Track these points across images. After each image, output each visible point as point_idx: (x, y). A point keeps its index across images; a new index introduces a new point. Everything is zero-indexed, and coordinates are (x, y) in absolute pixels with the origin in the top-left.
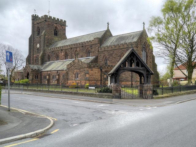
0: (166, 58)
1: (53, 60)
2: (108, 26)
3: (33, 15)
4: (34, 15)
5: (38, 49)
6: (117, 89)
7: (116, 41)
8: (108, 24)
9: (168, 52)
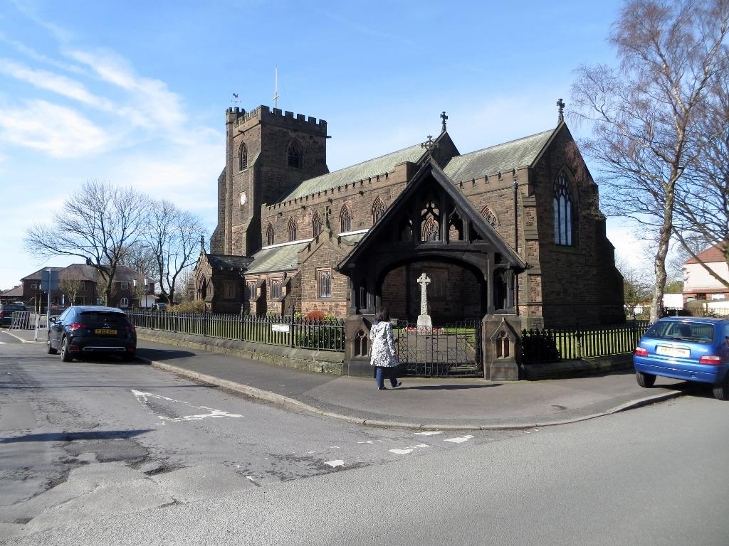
0: (646, 217)
2: (444, 123)
4: (233, 110)
7: (468, 171)
8: (444, 117)
9: (645, 196)
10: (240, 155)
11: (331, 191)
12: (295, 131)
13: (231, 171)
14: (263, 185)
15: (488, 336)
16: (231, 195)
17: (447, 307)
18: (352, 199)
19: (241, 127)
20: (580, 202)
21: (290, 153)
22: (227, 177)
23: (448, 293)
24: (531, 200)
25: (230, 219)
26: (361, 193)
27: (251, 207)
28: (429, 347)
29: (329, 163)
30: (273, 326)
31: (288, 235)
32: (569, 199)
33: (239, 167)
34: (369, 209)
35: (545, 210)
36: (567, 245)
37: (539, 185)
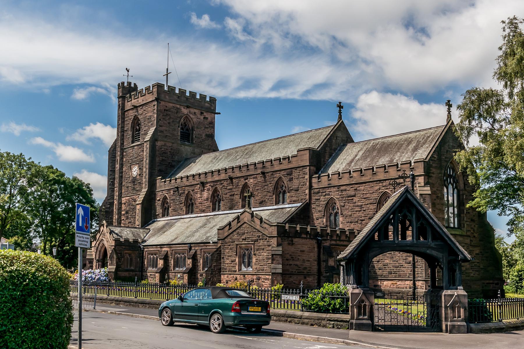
2: (340, 112)
3: (123, 83)
4: (126, 84)
5: (134, 180)
10: (133, 127)
12: (188, 107)
13: (122, 144)
14: (157, 159)
15: (446, 304)
16: (122, 165)
18: (254, 178)
19: (134, 102)
20: (465, 190)
21: (182, 129)
24: (426, 188)
25: (120, 189)
26: (263, 173)
27: (145, 180)
31: (184, 209)
32: (456, 187)
34: (271, 189)
35: (438, 197)
36: (454, 228)
37: (432, 175)
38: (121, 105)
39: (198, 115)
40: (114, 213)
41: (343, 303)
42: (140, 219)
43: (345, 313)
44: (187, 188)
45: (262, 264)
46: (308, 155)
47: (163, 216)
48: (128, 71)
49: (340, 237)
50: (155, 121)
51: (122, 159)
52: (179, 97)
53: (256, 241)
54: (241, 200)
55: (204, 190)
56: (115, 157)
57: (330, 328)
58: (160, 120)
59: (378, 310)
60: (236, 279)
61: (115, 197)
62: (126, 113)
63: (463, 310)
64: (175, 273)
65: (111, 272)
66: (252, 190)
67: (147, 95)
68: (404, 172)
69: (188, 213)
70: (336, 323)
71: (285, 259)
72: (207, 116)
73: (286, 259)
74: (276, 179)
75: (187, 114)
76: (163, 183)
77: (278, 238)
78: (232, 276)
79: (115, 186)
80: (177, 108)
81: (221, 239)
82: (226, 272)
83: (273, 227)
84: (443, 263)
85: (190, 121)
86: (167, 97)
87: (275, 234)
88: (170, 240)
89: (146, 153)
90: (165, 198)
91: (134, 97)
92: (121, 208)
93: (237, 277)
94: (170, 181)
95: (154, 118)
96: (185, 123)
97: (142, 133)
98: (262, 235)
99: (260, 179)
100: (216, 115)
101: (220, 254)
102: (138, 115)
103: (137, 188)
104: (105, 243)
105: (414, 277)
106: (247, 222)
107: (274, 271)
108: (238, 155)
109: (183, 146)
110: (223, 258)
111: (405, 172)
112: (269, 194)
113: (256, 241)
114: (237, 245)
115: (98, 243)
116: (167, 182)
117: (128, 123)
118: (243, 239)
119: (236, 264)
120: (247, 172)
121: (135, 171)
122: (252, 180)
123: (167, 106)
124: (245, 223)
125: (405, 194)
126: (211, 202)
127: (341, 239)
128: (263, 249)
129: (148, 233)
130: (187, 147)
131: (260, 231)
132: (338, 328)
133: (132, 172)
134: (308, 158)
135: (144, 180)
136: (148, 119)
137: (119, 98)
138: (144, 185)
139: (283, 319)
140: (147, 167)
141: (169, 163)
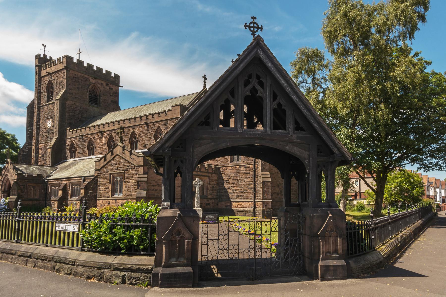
1: (82, 154)
3: (39, 55)
5: (49, 131)
6: (179, 233)
11: (123, 121)
12: (95, 78)
14: (67, 114)
17: (207, 202)
18: (140, 127)
19: (49, 70)
21: (90, 94)
22: (36, 106)
23: (209, 193)
25: (38, 137)
26: (147, 124)
27: (56, 130)
28: (252, 244)
29: (120, 104)
30: (57, 225)
31: (87, 152)
33: (46, 99)
34: (152, 135)
38: (37, 72)
39: (104, 86)
40: (32, 156)
41: (146, 234)
42: (50, 159)
43: (149, 253)
44: (89, 136)
45: (130, 190)
46: (179, 109)
47: (71, 157)
48: (45, 47)
49: (200, 169)
50: (65, 85)
51: (39, 114)
52: (87, 69)
53: (126, 170)
54: (130, 145)
55: (102, 137)
56: (33, 113)
57: (117, 284)
58: (70, 84)
59: (208, 245)
60: (109, 204)
61: (33, 144)
62: (42, 79)
63: (341, 239)
64: (72, 200)
65: (12, 201)
66: (139, 137)
67: (58, 64)
68: (254, 20)
69: (90, 155)
70: (128, 274)
71: (151, 185)
72: (112, 88)
73: (152, 185)
74: (156, 128)
75: (95, 83)
76: (71, 133)
77: (144, 168)
78: (106, 201)
79: (34, 135)
80: (85, 77)
81: (98, 170)
82: (101, 198)
83: (140, 158)
84: (310, 166)
85: (97, 89)
86: (76, 67)
87: (142, 164)
88: (70, 174)
89: (56, 109)
90: (72, 144)
91: (48, 66)
92: (38, 152)
93: (109, 202)
94: (77, 131)
95: (64, 82)
96: (93, 90)
97: (55, 94)
98: (131, 165)
99: (144, 128)
100: (120, 88)
101: (96, 183)
102: (52, 80)
103: (51, 136)
104: (9, 177)
105: (255, 199)
106: (119, 154)
107: (139, 195)
108: (131, 113)
109: (91, 107)
110: (99, 186)
111: (255, 21)
112: (151, 140)
113: (126, 170)
114: (110, 174)
115: (3, 177)
116: (74, 132)
117: (44, 86)
118: (116, 169)
119: (109, 191)
120: (134, 123)
121: (49, 124)
122: (138, 129)
123: (76, 75)
124: (117, 155)
125: (255, 51)
126: (107, 146)
127: (201, 171)
128: (132, 177)
129: (55, 170)
130: (94, 108)
131: (129, 162)
132: (131, 284)
133: (47, 124)
134: (179, 111)
135: (55, 130)
136: (59, 83)
137: (36, 66)
138: (55, 134)
139: (49, 265)
140: (58, 119)
141: (79, 118)
